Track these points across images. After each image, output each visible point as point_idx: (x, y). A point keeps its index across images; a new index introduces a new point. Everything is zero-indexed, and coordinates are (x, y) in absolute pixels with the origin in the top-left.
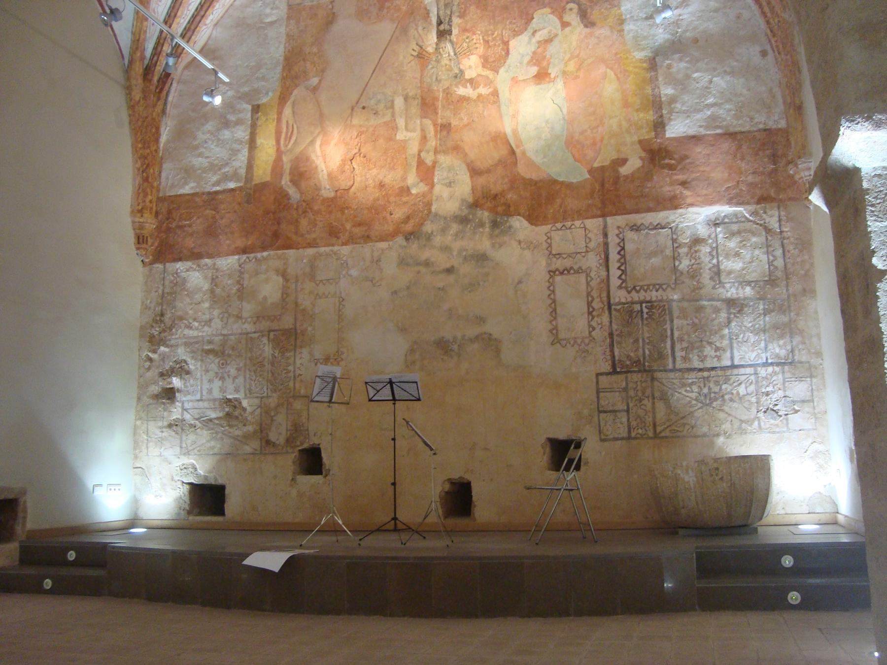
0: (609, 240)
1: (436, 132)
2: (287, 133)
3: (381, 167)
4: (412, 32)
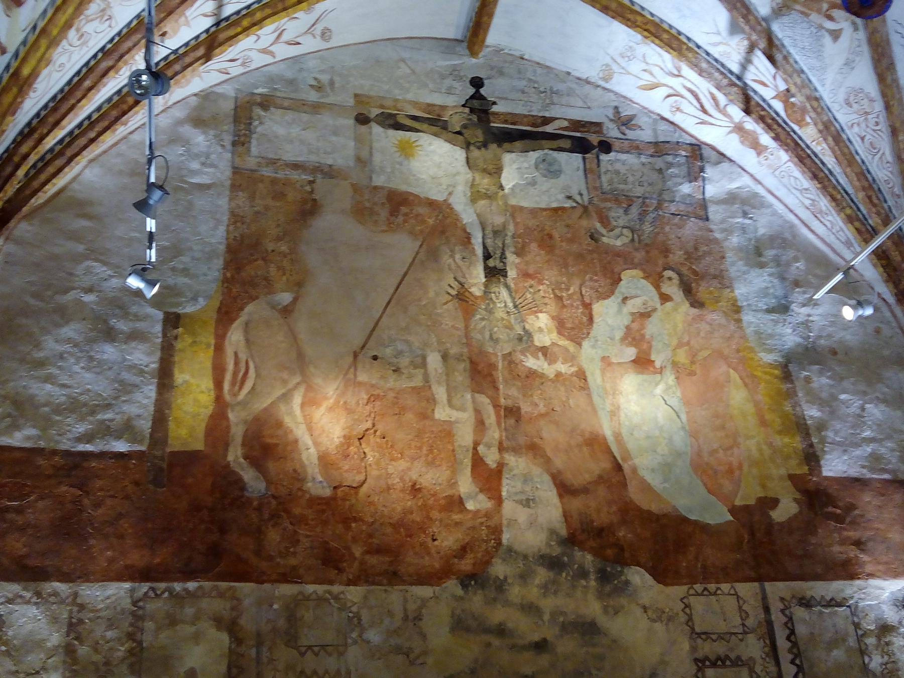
0: (773, 618)
1: (498, 416)
2: (235, 374)
3: (413, 459)
4: (446, 259)
